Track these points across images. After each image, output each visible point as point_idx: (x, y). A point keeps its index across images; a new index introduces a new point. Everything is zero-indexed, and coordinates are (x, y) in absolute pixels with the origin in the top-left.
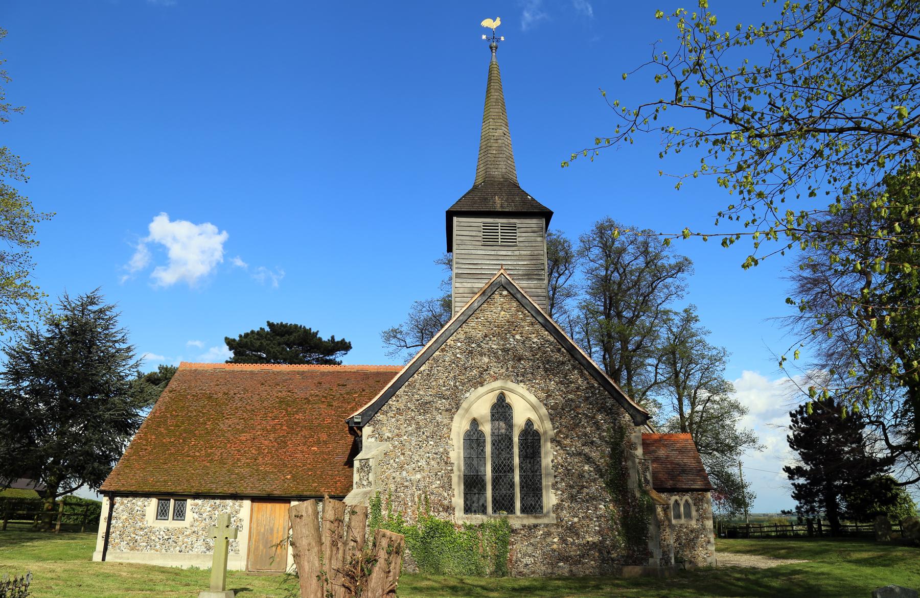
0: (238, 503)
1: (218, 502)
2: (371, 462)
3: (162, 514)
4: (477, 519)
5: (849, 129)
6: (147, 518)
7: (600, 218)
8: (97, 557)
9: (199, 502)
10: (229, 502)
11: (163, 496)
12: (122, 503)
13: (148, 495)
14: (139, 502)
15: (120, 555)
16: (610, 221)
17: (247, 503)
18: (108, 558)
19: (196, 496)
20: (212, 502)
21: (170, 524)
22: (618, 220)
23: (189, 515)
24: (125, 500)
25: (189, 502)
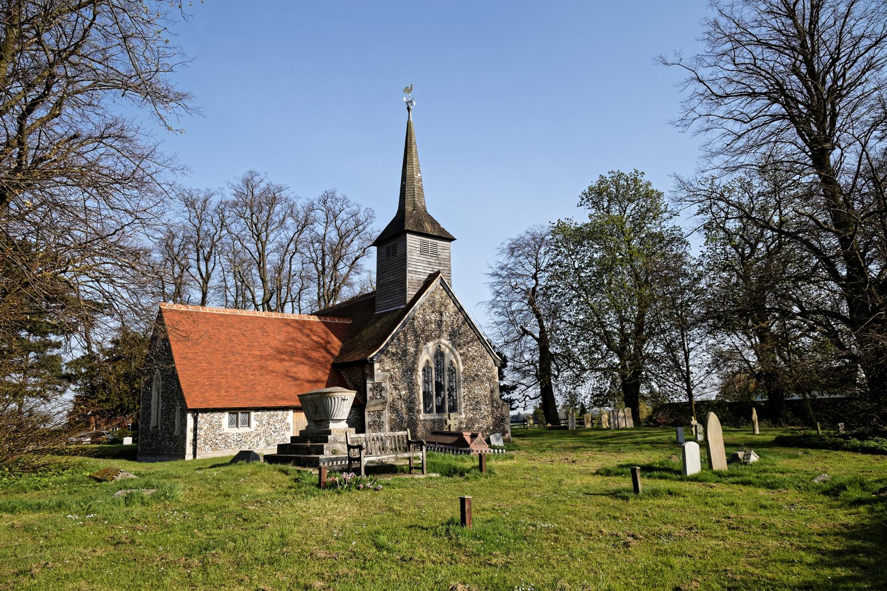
0: (285, 412)
1: (272, 413)
2: (383, 385)
3: (231, 423)
4: (429, 417)
5: (859, 167)
6: (223, 427)
7: (329, 188)
8: (189, 456)
9: (260, 413)
10: (280, 413)
11: (233, 411)
12: (202, 418)
13: (222, 410)
14: (216, 416)
15: (206, 453)
16: (251, 172)
17: (291, 412)
18: (198, 457)
19: (257, 409)
20: (268, 413)
21: (243, 430)
22: (257, 169)
23: (254, 423)
24: (205, 415)
25: (253, 414)
